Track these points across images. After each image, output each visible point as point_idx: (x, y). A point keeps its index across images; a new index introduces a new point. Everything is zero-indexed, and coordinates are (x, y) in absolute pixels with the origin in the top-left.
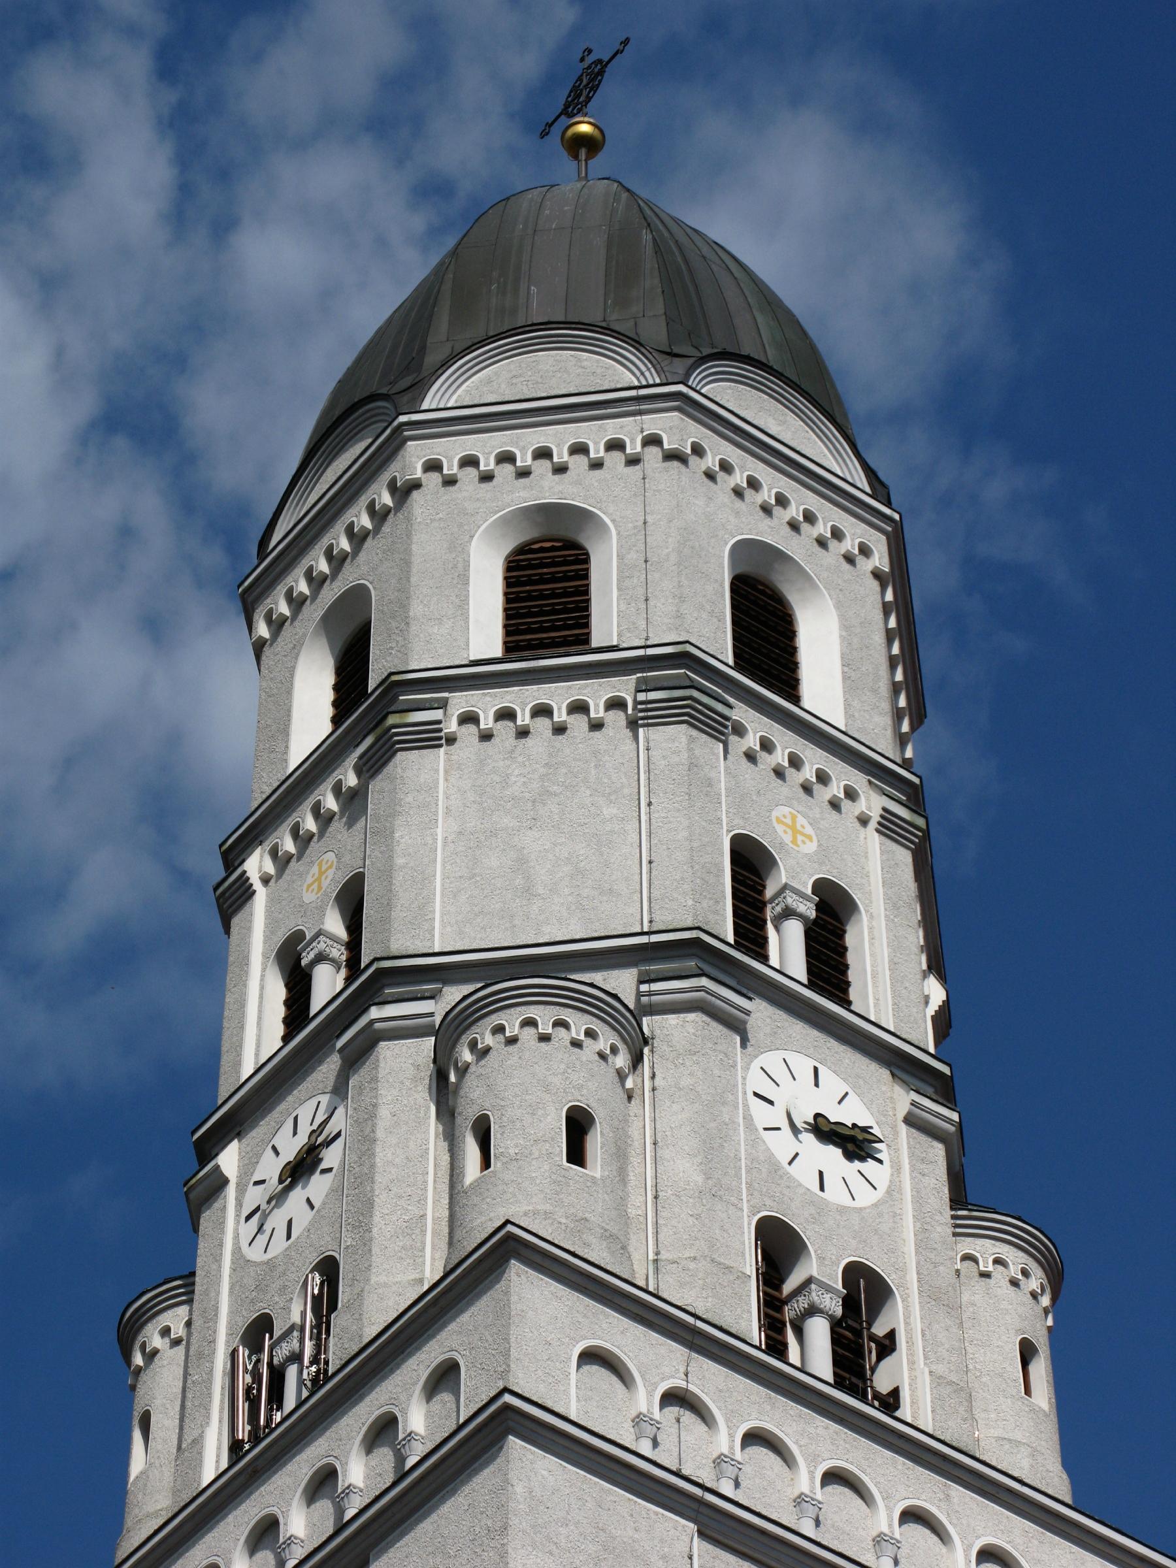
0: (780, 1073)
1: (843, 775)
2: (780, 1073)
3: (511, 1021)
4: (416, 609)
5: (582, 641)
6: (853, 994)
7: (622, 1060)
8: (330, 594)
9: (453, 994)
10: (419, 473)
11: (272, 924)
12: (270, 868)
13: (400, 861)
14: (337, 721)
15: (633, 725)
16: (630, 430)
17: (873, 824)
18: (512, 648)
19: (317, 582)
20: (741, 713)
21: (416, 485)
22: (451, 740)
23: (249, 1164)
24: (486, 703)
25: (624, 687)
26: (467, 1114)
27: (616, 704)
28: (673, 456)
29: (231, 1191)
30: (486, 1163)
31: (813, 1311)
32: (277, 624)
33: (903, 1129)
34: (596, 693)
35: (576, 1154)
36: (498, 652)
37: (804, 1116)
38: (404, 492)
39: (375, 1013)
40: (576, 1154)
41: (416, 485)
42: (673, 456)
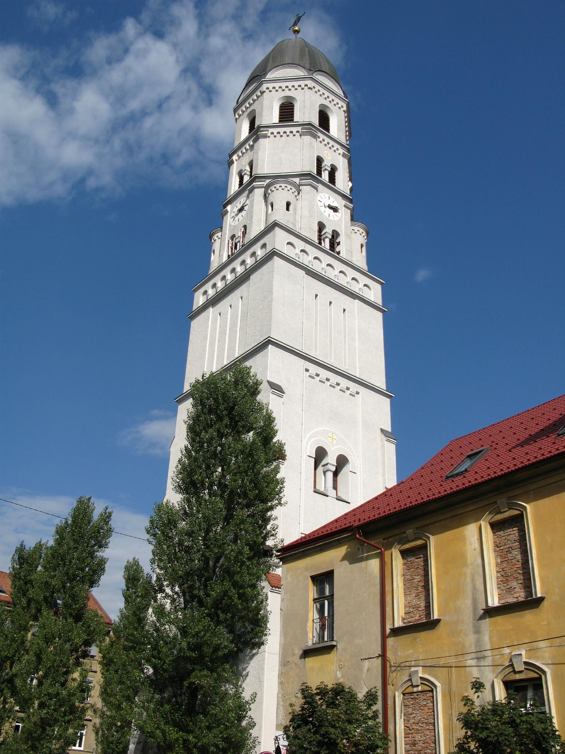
0: (323, 197)
1: (336, 146)
2: (323, 197)
3: (277, 186)
4: (264, 114)
5: (292, 120)
6: (336, 184)
7: (296, 194)
8: (249, 110)
9: (268, 181)
10: (265, 90)
11: (237, 168)
12: (237, 158)
13: (259, 158)
14: (249, 133)
15: (301, 135)
16: (302, 83)
17: (341, 155)
18: (280, 121)
19: (247, 108)
20: (319, 134)
21: (264, 92)
22: (269, 137)
23: (232, 209)
24: (275, 131)
25: (299, 129)
26: (269, 201)
27: (298, 132)
28: (310, 88)
29: (229, 213)
30: (272, 210)
31: (326, 237)
32: (239, 116)
33: (344, 207)
34: (294, 130)
35: (288, 209)
36: (278, 122)
37: (327, 205)
38: (262, 93)
39: (254, 184)
40: (288, 209)
41: (264, 92)
42: (310, 88)
